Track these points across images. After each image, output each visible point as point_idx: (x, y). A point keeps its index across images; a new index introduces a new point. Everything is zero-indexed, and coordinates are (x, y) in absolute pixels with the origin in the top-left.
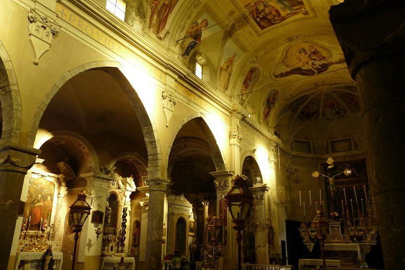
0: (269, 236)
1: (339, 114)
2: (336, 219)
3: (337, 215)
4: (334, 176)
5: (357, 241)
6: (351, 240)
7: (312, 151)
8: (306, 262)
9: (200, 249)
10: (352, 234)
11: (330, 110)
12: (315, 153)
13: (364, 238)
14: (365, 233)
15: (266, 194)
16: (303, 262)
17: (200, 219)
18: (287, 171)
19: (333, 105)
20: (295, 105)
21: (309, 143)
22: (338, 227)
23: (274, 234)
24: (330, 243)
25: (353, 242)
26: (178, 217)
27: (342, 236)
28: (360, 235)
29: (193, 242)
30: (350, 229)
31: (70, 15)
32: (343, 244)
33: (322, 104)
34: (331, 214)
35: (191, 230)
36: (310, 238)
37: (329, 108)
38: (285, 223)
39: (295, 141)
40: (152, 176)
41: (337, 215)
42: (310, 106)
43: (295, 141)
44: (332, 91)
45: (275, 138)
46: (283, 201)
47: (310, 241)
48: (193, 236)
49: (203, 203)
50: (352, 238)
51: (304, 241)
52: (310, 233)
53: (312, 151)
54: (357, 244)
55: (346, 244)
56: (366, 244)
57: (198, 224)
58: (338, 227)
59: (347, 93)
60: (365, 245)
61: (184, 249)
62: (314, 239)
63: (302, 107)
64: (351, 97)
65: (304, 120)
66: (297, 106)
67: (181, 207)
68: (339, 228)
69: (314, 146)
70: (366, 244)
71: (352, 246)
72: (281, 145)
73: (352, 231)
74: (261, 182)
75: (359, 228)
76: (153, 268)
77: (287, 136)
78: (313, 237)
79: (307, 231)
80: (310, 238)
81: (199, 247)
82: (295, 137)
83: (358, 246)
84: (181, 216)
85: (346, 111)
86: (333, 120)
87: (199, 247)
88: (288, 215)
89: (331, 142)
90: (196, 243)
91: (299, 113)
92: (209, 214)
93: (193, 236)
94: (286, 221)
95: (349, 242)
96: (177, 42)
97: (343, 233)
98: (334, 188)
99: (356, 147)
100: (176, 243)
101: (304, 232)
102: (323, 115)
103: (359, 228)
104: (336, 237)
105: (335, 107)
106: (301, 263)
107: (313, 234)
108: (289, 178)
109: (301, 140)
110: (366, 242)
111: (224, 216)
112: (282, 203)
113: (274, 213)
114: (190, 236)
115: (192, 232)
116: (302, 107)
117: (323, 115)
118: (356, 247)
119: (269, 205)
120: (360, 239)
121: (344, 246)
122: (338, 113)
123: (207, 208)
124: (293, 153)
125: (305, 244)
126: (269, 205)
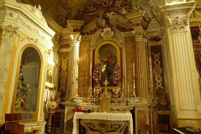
9: (64, 108)
17: (64, 67)
26: (26, 42)
29: (51, 98)
35: (49, 79)
40: (23, 107)
48: (51, 89)
49: (72, 37)
57: (60, 70)
61: (35, 108)
67: (33, 26)
76: (106, 66)
81: (61, 107)
84: (31, 42)
87: (61, 107)
90: (55, 100)
92: (80, 56)
93: (51, 89)
96: (31, 11)
98: (98, 85)
100: (17, 96)
111: (178, 7)
114: (46, 87)
115: (50, 82)
123: (77, 45)
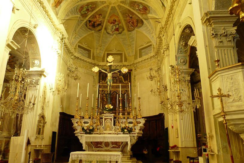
0: (38, 126)
1: (118, 31)
2: (110, 111)
3: (112, 107)
4: (112, 72)
5: (128, 132)
6: (122, 131)
7: (92, 58)
8: (80, 156)
10: (123, 126)
11: (112, 25)
12: (93, 59)
13: (134, 130)
14: (134, 126)
15: (43, 81)
16: (76, 156)
18: (68, 69)
19: (115, 21)
20: (85, 9)
21: (89, 51)
22: (111, 119)
23: (45, 123)
24: (102, 134)
25: (124, 134)
27: (114, 128)
28: (130, 127)
30: (121, 121)
31: (36, 145)
32: (114, 135)
33: (106, 18)
34: (106, 106)
36: (83, 129)
37: (111, 23)
38: (59, 115)
39: (79, 47)
41: (112, 107)
42: (97, 16)
43: (79, 47)
44: (119, 6)
45: (62, 28)
46: (60, 88)
47: (83, 132)
50: (123, 130)
51: (76, 132)
52: (83, 124)
53: (92, 58)
54: (128, 135)
55: (116, 135)
56: (134, 135)
58: (111, 119)
59: (129, 10)
60: (134, 136)
62: (87, 130)
63: (90, 14)
64: (131, 16)
65: (90, 29)
66: (86, 12)
68: (111, 121)
69: (93, 54)
70: (134, 135)
71: (123, 137)
72: (66, 41)
73: (123, 123)
74: (39, 66)
75: (129, 120)
77: (72, 40)
78: (85, 128)
79: (81, 122)
80: (83, 129)
82: (79, 42)
83: (129, 137)
85: (123, 30)
86: (113, 35)
88: (62, 108)
89: (107, 54)
91: (87, 21)
94: (60, 113)
95: (119, 134)
97: (114, 125)
99: (126, 60)
101: (77, 123)
102: (106, 29)
103: (129, 120)
104: (108, 129)
105: (116, 23)
106: (73, 156)
107: (86, 125)
108: (69, 75)
109: (84, 47)
110: (134, 134)
112: (59, 91)
113: (48, 102)
116: (90, 14)
117: (106, 29)
118: (126, 138)
119: (45, 92)
120: (130, 131)
121: (116, 138)
122: (117, 30)
124: (76, 54)
125: (76, 135)
126: (45, 92)
